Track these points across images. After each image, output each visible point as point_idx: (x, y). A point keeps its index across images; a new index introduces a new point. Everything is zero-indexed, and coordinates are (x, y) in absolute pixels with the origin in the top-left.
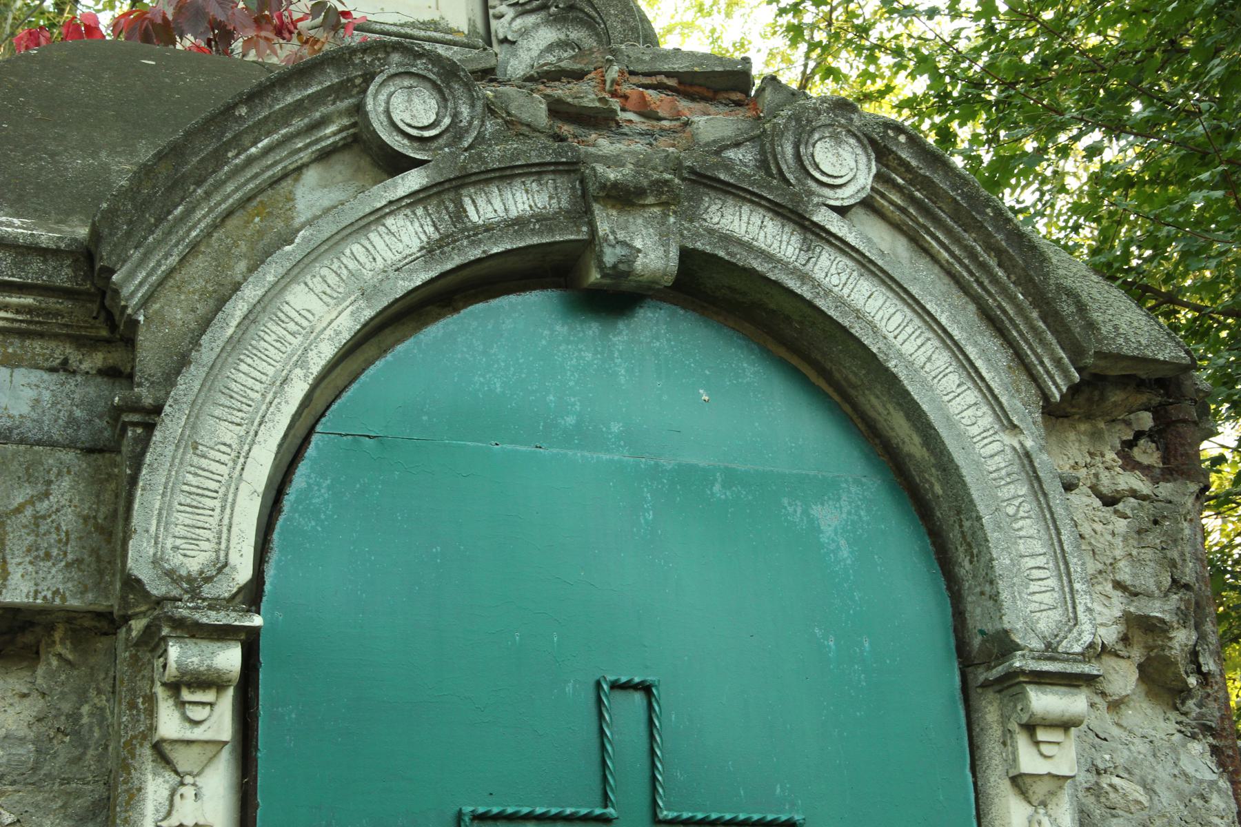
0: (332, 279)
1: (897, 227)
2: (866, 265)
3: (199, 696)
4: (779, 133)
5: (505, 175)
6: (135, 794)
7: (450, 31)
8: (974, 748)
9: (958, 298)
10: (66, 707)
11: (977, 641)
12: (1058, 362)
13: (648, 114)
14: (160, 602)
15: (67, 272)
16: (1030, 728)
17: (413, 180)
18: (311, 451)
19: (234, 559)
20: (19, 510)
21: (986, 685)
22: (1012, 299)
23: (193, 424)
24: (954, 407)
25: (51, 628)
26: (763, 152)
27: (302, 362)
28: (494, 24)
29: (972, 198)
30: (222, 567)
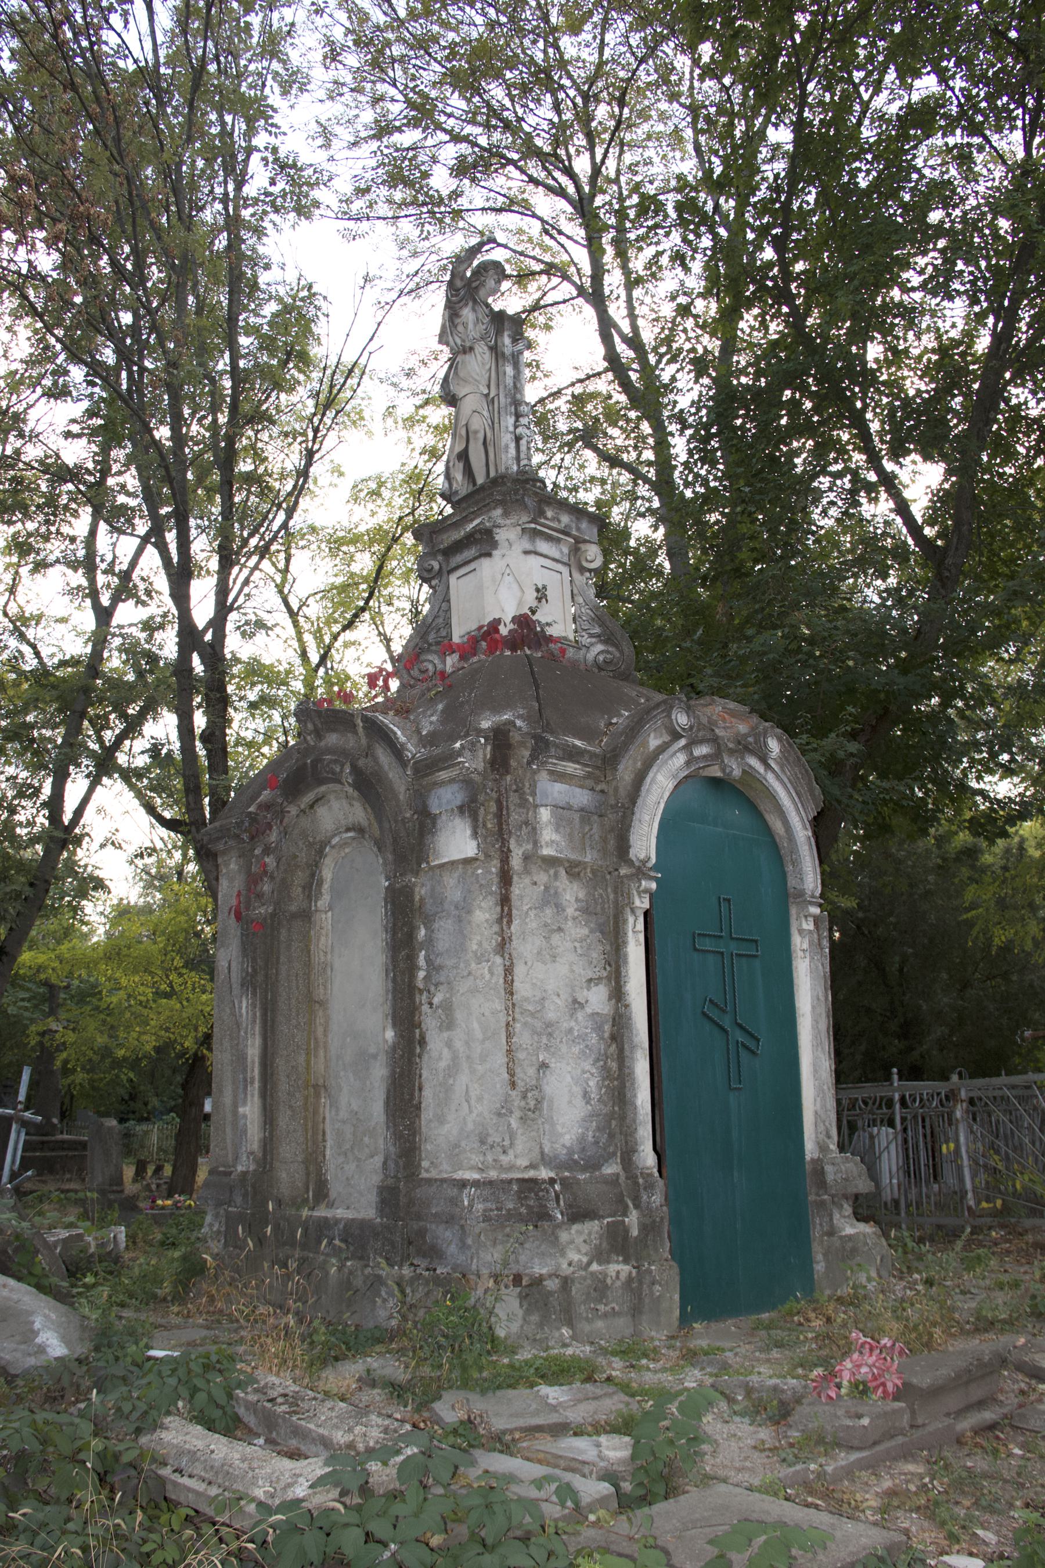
6: (625, 921)
17: (683, 742)
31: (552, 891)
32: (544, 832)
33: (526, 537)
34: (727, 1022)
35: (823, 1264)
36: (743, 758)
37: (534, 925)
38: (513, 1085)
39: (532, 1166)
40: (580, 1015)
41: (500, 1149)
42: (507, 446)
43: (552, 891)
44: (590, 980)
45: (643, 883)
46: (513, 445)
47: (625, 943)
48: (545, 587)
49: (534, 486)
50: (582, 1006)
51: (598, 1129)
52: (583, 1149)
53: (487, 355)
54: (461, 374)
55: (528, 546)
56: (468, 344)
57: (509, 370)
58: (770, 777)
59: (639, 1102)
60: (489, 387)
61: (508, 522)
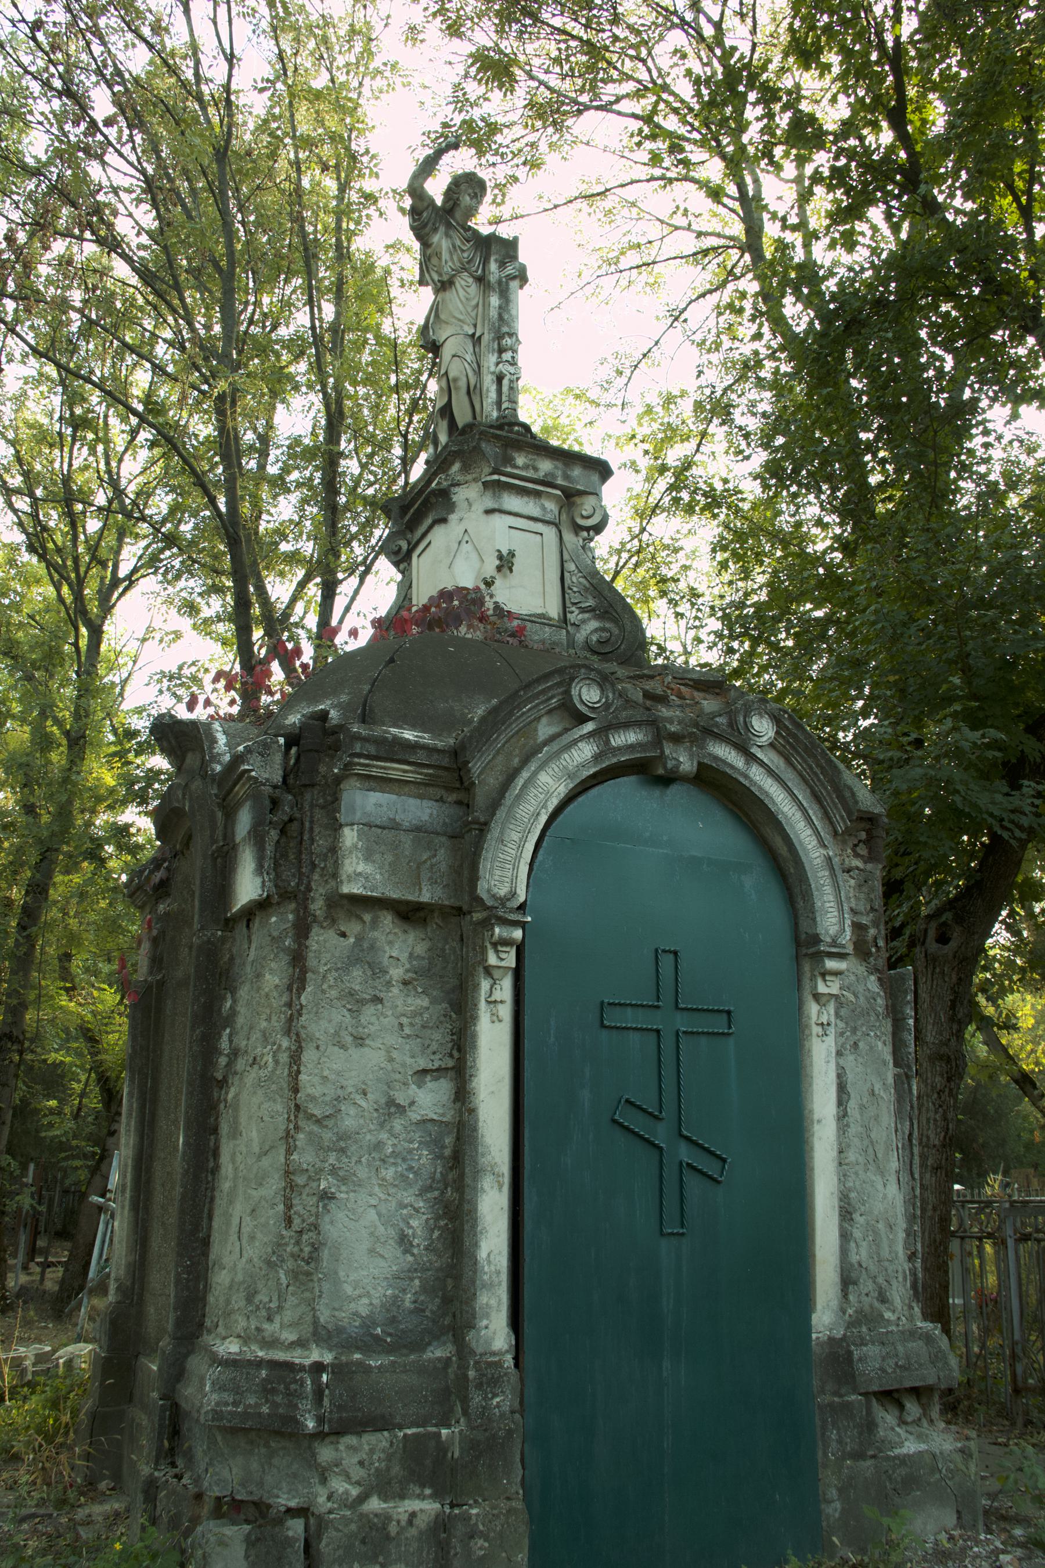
0: (556, 769)
1: (780, 753)
2: (770, 772)
3: (504, 949)
4: (737, 711)
5: (626, 725)
6: (477, 987)
7: (550, 619)
8: (799, 981)
9: (803, 786)
10: (440, 945)
11: (803, 936)
12: (842, 817)
13: (681, 697)
14: (489, 908)
15: (447, 760)
16: (823, 975)
17: (590, 727)
18: (545, 844)
19: (518, 891)
20: (425, 862)
21: (806, 955)
22: (826, 788)
23: (502, 833)
24: (802, 836)
25: (432, 911)
26: (730, 719)
27: (545, 806)
28: (569, 615)
29: (812, 743)
30: (513, 894)
31: (365, 945)
32: (347, 862)
33: (489, 494)
34: (661, 1134)
35: (838, 1505)
36: (702, 747)
37: (334, 993)
38: (289, 1221)
39: (301, 1344)
40: (398, 1124)
41: (264, 1313)
42: (488, 391)
43: (365, 945)
44: (425, 1071)
45: (497, 930)
46: (494, 388)
47: (474, 1018)
48: (511, 553)
49: (511, 431)
50: (401, 1110)
51: (424, 1289)
52: (393, 1320)
53: (473, 289)
54: (443, 317)
55: (490, 504)
56: (445, 278)
57: (495, 301)
58: (756, 774)
59: (483, 1254)
60: (475, 326)
61: (469, 477)
